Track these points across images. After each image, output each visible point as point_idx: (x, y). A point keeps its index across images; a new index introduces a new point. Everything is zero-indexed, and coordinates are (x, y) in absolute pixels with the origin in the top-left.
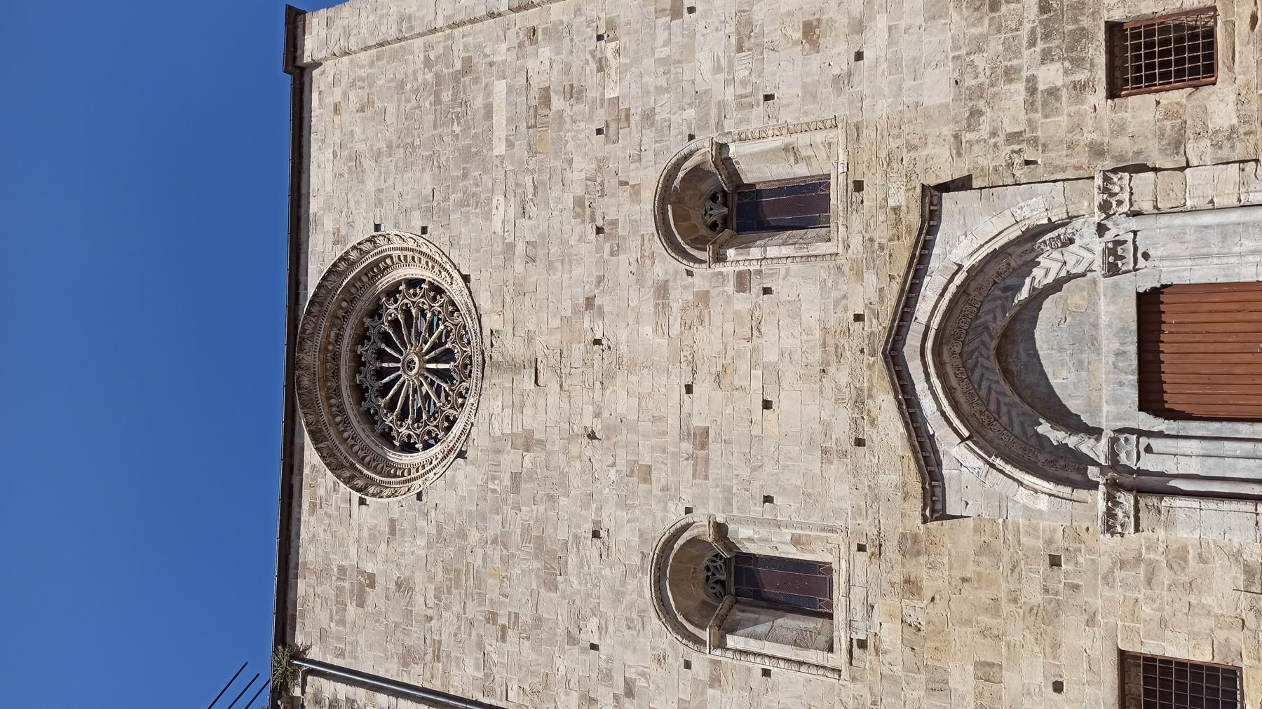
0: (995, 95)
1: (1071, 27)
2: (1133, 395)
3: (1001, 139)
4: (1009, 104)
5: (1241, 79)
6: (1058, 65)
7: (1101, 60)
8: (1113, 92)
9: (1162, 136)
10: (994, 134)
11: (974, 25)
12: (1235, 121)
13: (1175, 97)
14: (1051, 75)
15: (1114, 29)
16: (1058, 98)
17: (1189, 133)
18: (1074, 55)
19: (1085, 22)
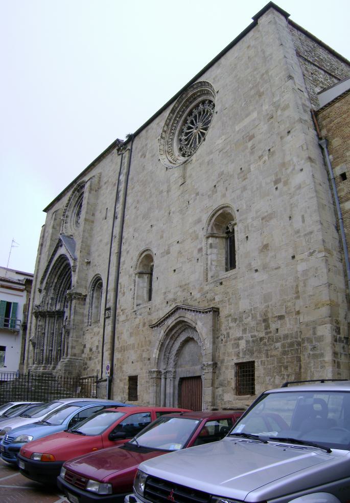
0: (240, 326)
1: (255, 349)
2: (182, 376)
3: (228, 331)
4: (237, 331)
5: (234, 402)
6: (245, 346)
7: (245, 360)
8: (237, 364)
9: (224, 381)
10: (230, 328)
11: (260, 314)
12: (225, 400)
13: (233, 385)
14: (243, 344)
15: (254, 362)
16: (236, 348)
17: (224, 388)
18: (247, 351)
19: (255, 354)
